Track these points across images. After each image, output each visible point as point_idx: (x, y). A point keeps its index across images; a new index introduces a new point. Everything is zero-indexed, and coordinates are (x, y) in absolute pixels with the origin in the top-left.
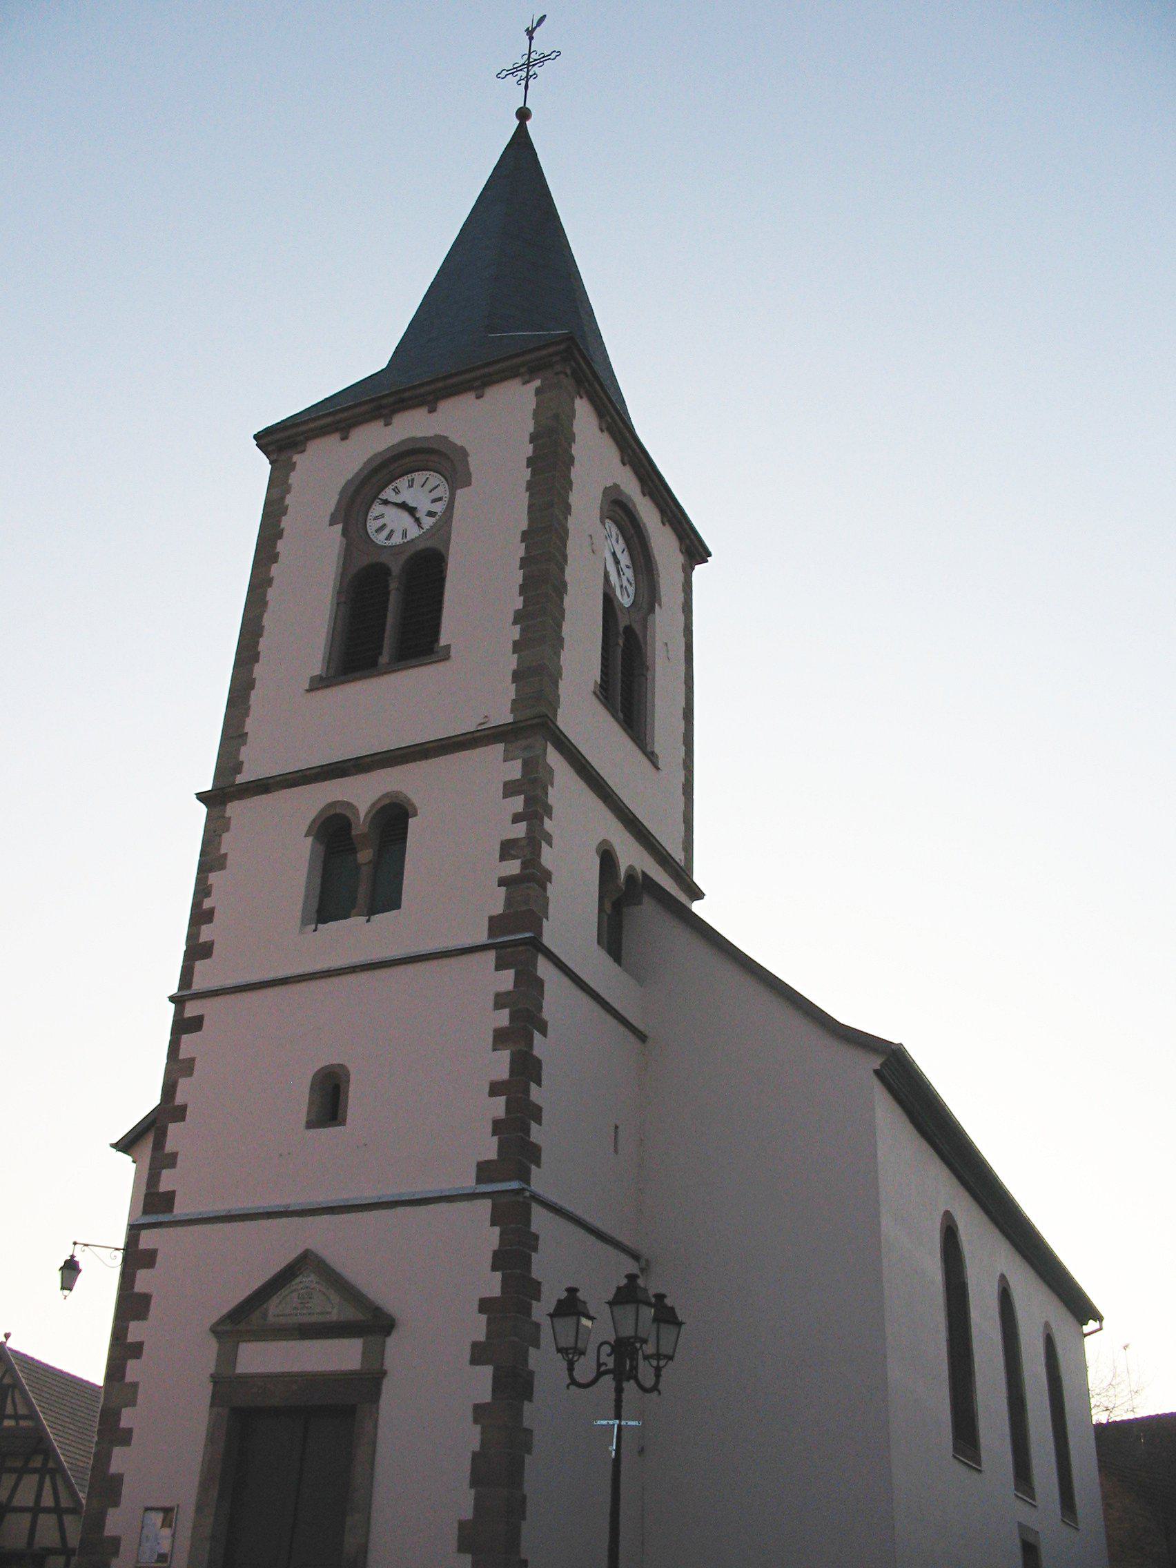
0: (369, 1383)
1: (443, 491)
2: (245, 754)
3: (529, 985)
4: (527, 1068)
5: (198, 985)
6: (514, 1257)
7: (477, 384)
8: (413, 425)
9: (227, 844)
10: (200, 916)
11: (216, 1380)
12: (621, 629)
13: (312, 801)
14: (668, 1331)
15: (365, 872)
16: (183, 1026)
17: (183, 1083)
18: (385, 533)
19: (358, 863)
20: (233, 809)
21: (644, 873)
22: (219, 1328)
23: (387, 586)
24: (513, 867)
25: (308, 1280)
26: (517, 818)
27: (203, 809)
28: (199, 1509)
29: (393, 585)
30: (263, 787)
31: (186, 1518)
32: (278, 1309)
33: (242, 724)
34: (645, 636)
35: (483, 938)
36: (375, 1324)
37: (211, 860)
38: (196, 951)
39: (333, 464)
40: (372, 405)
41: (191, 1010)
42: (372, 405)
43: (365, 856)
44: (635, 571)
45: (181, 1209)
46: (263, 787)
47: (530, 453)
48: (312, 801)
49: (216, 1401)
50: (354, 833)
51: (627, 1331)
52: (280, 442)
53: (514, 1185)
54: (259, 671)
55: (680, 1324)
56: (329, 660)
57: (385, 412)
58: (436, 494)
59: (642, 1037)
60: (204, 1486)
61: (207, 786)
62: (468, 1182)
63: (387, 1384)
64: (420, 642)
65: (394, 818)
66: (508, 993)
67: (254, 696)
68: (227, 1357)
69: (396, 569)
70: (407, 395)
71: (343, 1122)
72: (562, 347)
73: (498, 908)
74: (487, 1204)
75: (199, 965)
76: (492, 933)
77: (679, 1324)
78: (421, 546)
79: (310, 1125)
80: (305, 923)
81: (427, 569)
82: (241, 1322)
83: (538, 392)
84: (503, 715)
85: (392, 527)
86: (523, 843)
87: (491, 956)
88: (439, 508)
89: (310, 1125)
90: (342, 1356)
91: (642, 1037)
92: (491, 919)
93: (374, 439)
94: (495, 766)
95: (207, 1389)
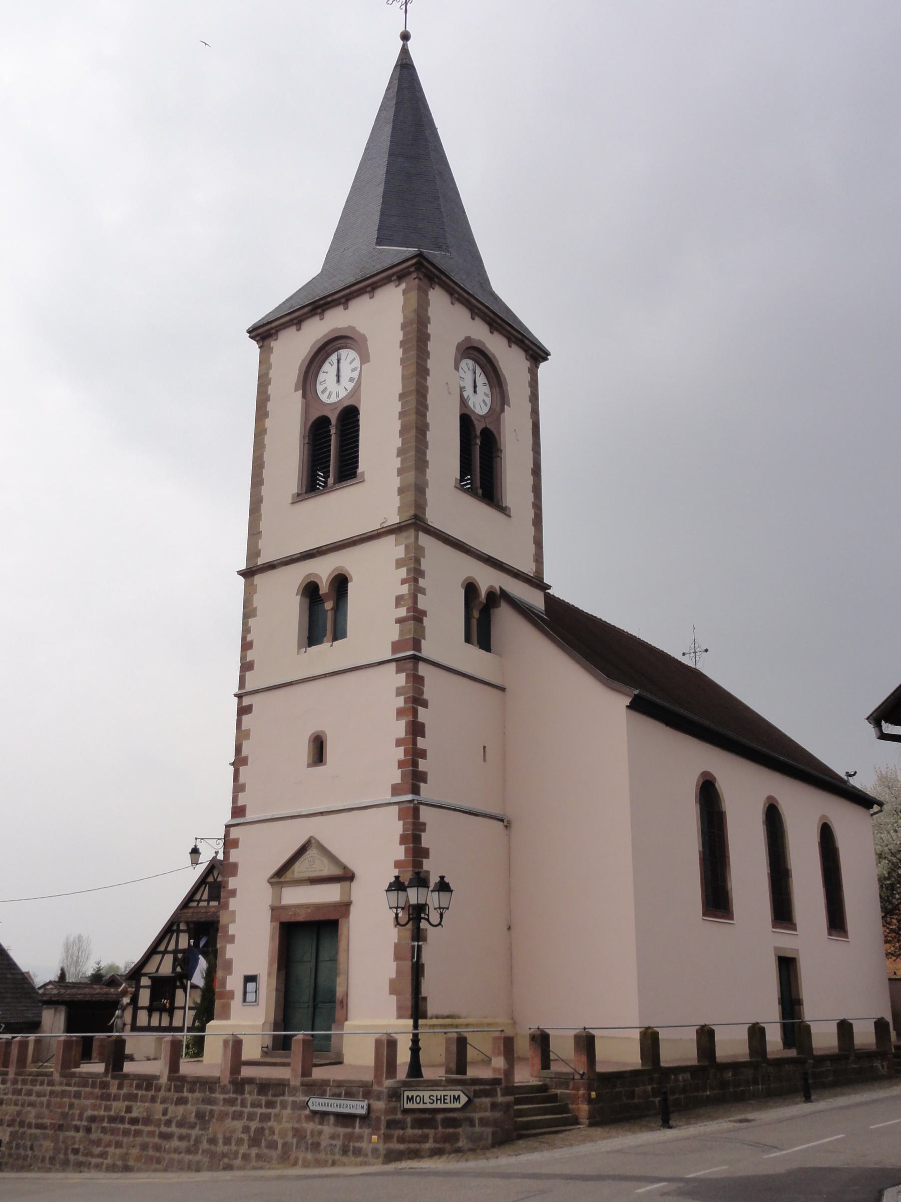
0: (345, 907)
1: (357, 363)
2: (262, 544)
3: (417, 681)
4: (416, 729)
5: (249, 687)
6: (413, 838)
7: (369, 289)
8: (335, 320)
9: (257, 601)
10: (246, 646)
11: (273, 909)
12: (478, 433)
13: (298, 574)
14: (444, 895)
15: (330, 615)
16: (243, 711)
17: (246, 745)
18: (327, 393)
19: (324, 610)
20: (258, 579)
21: (501, 588)
22: (273, 880)
23: (330, 431)
24: (402, 612)
25: (312, 853)
26: (403, 582)
27: (242, 580)
28: (269, 975)
29: (333, 431)
30: (271, 566)
31: (263, 981)
32: (301, 869)
33: (258, 525)
34: (499, 433)
35: (389, 656)
36: (346, 877)
37: (249, 612)
38: (246, 666)
39: (296, 345)
40: (309, 308)
41: (246, 701)
42: (309, 308)
43: (329, 605)
44: (491, 388)
45: (249, 817)
46: (271, 566)
47: (401, 338)
48: (298, 574)
49: (273, 919)
50: (321, 593)
51: (422, 902)
52: (264, 333)
53: (409, 797)
54: (265, 490)
55: (452, 891)
56: (301, 484)
57: (319, 311)
58: (327, 393)
59: (503, 689)
60: (270, 965)
61: (243, 566)
62: (388, 797)
63: (353, 909)
64: (348, 471)
65: (341, 583)
66: (403, 687)
67: (264, 507)
68: (278, 896)
69: (334, 421)
70: (329, 299)
71: (325, 764)
72: (414, 261)
73: (396, 637)
74: (396, 808)
75: (248, 675)
76: (394, 651)
77: (452, 891)
78: (346, 404)
79: (309, 766)
80: (300, 647)
81: (350, 416)
82: (281, 876)
83: (405, 292)
84: (394, 519)
85: (333, 389)
86: (407, 597)
87: (394, 665)
88: (355, 375)
89: (309, 766)
90: (330, 894)
91: (503, 689)
92: (393, 643)
93: (316, 330)
94: (392, 550)
95: (269, 913)
